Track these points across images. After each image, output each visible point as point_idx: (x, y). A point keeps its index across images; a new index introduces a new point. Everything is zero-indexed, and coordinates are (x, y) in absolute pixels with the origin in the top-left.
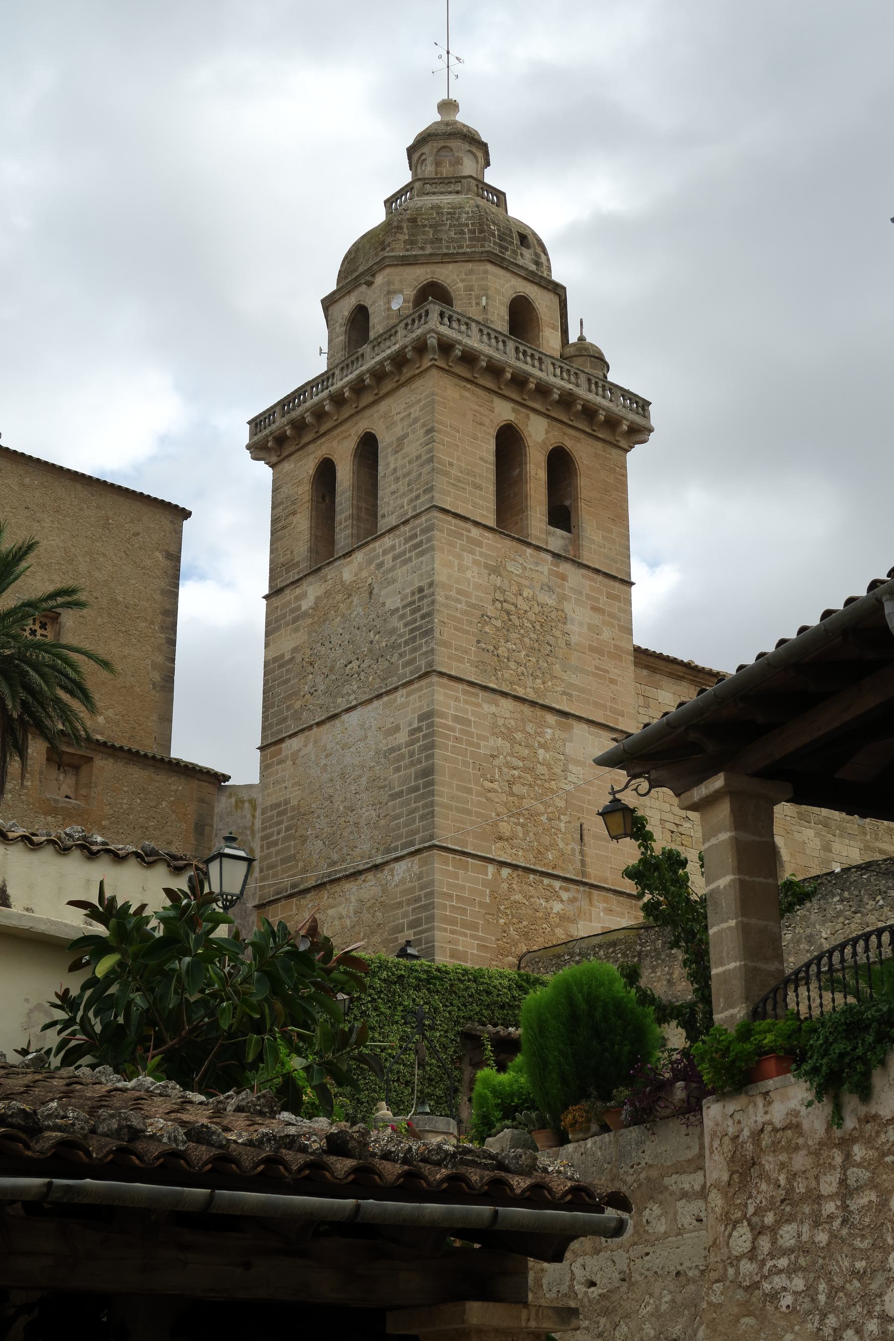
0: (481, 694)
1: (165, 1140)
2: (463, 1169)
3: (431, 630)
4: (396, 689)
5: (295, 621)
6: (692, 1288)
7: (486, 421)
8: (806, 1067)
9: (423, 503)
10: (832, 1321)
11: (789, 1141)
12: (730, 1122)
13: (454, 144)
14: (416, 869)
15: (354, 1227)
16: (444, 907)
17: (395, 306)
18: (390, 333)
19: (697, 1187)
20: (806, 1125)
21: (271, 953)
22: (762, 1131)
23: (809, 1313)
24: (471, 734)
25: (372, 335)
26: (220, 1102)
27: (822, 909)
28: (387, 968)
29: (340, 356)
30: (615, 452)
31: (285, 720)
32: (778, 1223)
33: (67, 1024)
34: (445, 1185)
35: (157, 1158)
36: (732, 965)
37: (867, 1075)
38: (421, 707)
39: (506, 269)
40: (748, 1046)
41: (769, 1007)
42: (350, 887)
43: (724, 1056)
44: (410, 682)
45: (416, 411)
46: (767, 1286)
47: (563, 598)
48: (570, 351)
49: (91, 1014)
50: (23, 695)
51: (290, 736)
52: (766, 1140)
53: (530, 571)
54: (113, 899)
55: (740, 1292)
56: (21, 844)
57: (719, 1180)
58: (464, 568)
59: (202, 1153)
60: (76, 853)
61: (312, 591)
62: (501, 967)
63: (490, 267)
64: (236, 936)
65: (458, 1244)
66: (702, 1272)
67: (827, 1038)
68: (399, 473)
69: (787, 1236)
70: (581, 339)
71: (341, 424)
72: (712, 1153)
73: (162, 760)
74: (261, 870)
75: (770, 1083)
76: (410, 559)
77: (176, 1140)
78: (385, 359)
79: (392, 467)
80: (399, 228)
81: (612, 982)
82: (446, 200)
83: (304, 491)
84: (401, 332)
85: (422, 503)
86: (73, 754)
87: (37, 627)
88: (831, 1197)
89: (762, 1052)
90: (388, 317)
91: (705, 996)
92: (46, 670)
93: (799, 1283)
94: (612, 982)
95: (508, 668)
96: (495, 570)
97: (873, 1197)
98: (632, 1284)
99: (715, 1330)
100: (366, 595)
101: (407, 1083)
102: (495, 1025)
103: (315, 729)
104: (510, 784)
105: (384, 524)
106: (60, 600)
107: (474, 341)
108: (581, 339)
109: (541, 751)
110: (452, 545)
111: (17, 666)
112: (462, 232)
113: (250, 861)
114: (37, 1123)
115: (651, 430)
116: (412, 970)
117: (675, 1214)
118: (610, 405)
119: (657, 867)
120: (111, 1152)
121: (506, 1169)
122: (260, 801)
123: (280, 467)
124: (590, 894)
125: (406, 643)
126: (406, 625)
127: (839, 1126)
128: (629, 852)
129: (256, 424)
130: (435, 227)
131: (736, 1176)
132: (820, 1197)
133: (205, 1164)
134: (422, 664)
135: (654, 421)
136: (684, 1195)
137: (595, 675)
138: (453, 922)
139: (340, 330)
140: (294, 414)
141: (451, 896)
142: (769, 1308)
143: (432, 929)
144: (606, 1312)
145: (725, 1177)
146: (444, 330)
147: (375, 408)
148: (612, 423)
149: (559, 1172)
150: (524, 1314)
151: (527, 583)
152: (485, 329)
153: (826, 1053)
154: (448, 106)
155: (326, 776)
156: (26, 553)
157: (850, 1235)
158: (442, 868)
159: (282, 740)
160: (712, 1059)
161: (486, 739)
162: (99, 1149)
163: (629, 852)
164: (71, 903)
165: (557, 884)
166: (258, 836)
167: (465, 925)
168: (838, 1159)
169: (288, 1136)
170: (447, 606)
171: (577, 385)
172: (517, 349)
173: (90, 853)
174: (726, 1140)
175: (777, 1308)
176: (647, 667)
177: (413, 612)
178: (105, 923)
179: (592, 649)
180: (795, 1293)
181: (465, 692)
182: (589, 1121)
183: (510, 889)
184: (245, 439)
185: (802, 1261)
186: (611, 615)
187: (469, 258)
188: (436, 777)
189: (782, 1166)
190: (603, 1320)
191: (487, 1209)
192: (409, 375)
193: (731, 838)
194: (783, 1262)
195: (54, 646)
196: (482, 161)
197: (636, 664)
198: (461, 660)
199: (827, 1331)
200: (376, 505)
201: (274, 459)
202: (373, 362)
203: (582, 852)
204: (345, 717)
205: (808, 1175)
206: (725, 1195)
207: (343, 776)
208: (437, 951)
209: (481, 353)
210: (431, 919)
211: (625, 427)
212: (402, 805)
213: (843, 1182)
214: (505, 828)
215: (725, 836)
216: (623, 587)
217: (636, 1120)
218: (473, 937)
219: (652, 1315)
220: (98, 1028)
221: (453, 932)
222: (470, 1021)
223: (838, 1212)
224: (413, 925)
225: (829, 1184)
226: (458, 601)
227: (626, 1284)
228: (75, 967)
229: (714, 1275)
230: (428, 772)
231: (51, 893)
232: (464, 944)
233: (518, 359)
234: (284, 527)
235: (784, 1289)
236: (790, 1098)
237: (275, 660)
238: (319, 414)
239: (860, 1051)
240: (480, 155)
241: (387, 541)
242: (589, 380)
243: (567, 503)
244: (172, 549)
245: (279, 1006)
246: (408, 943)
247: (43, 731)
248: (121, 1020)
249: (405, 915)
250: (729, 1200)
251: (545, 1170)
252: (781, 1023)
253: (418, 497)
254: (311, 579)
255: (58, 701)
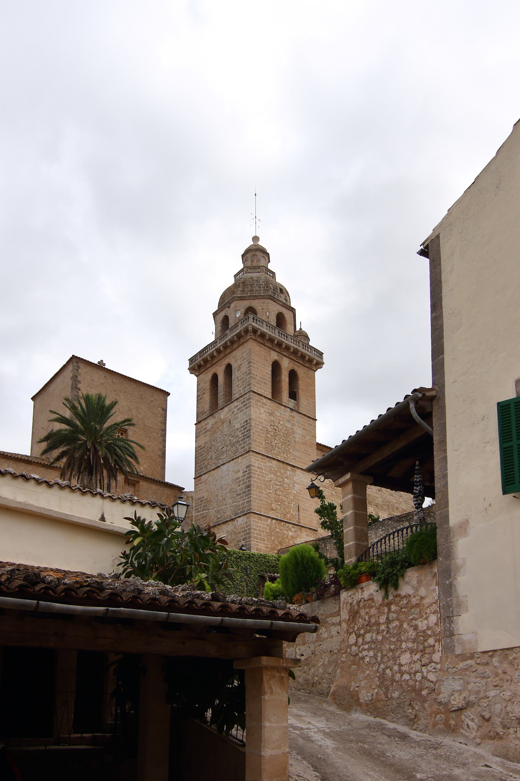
0: (266, 459)
1: (151, 594)
2: (260, 607)
3: (250, 436)
4: (238, 457)
5: (205, 433)
6: (335, 656)
7: (268, 359)
8: (376, 578)
9: (247, 389)
10: (382, 666)
11: (369, 604)
12: (350, 598)
13: (259, 254)
14: (245, 520)
15: (221, 628)
16: (254, 533)
17: (238, 316)
18: (236, 326)
19: (338, 621)
20: (375, 599)
21: (194, 537)
22: (360, 601)
23: (375, 663)
24: (263, 473)
25: (230, 327)
26: (176, 588)
27: (376, 534)
28: (236, 554)
29: (219, 335)
30: (311, 372)
31: (202, 468)
32: (365, 633)
33: (126, 563)
34: (254, 612)
35: (148, 600)
36: (351, 543)
37: (397, 580)
38: (247, 463)
39: (275, 302)
40: (356, 571)
41: (363, 558)
42: (224, 526)
43: (348, 575)
44: (243, 454)
45: (245, 355)
46: (360, 655)
47: (293, 425)
48: (297, 334)
49: (133, 560)
50: (115, 457)
51: (204, 474)
52: (362, 604)
53: (282, 414)
54: (139, 517)
55: (352, 657)
56: (108, 499)
57: (345, 618)
58: (262, 413)
59: (165, 599)
60: (128, 503)
61: (211, 422)
62: (274, 554)
63: (270, 301)
64: (183, 531)
65: (257, 636)
66: (339, 651)
67: (384, 567)
68: (239, 378)
69: (368, 638)
70: (301, 329)
71: (220, 360)
72: (343, 609)
73: (162, 482)
74: (195, 521)
75: (364, 584)
76: (243, 410)
77: (155, 594)
78: (234, 336)
79: (237, 376)
80: (239, 285)
81: (310, 551)
82: (255, 275)
83: (207, 385)
84: (240, 325)
85: (247, 390)
86: (133, 480)
87: (120, 435)
88: (383, 624)
89: (361, 573)
90: (235, 320)
91: (342, 555)
92: (122, 448)
93: (371, 653)
94: (310, 551)
95: (275, 450)
96: (271, 414)
97: (398, 624)
98: (315, 655)
99: (343, 670)
100: (228, 423)
101: (242, 592)
102: (270, 573)
103: (212, 472)
104: (276, 491)
105: (234, 397)
106: (126, 423)
107: (264, 329)
108: (301, 329)
109: (286, 479)
110: (257, 405)
111: (113, 447)
112: (260, 287)
113: (187, 506)
114: (102, 586)
115: (323, 364)
116: (244, 554)
117: (330, 631)
118: (310, 354)
119: (326, 508)
120: (130, 597)
121: (276, 608)
122: (194, 497)
123: (199, 376)
124: (301, 529)
125: (242, 440)
126: (242, 434)
127: (387, 599)
128: (316, 503)
129: (191, 360)
130: (251, 285)
131: (351, 617)
132: (380, 624)
133: (166, 603)
134: (247, 448)
135: (325, 360)
136: (334, 624)
137: (303, 452)
138: (257, 538)
139: (219, 325)
140: (204, 357)
141: (256, 529)
142: (361, 662)
143: (250, 541)
144: (307, 665)
145: (348, 618)
146: (254, 324)
147: (231, 354)
148: (310, 361)
149: (294, 609)
150: (282, 661)
151: (282, 419)
152: (268, 324)
153: (383, 573)
154: (256, 239)
155: (216, 488)
156: (114, 405)
157: (389, 636)
158: (254, 519)
159: (201, 476)
160: (344, 576)
161: (268, 475)
162: (125, 597)
163: (316, 503)
164: (125, 518)
165: (291, 526)
166: (194, 509)
167: (261, 539)
168: (386, 610)
169: (197, 594)
170: (255, 427)
171: (299, 346)
172: (279, 332)
173: (133, 503)
174: (348, 605)
175: (364, 662)
176: (320, 450)
177: (244, 429)
178: (137, 526)
179: (303, 443)
180: (370, 657)
181: (261, 458)
182: (302, 599)
183: (275, 527)
184: (187, 365)
185: (373, 646)
186: (309, 431)
187: (263, 297)
188: (252, 488)
189: (367, 613)
190: (306, 667)
191: (269, 621)
192: (242, 341)
193: (352, 497)
194: (366, 647)
195: (124, 440)
196: (267, 260)
197: (317, 449)
198: (259, 446)
199: (380, 670)
200: (231, 391)
201: (197, 374)
202: (230, 337)
203: (299, 515)
204: (222, 467)
205: (376, 616)
206: (347, 624)
207: (221, 488)
208: (252, 548)
209: (267, 333)
210: (250, 537)
211: (315, 362)
212: (240, 498)
213: (387, 618)
214: (274, 506)
215: (350, 496)
216: (313, 421)
217: (318, 599)
218: (264, 544)
219: (322, 665)
220: (136, 565)
221: (257, 542)
222: (262, 569)
223: (386, 629)
224: (244, 539)
225: (383, 619)
226: (259, 425)
227: (313, 655)
228: (128, 542)
229: (343, 651)
230: (249, 486)
231: (119, 517)
232: (261, 546)
233: (279, 336)
234: (201, 399)
235: (367, 656)
236: (371, 589)
237: (199, 447)
238: (212, 356)
239: (395, 572)
240: (267, 258)
241: (235, 403)
242: (303, 344)
243: (295, 390)
244: (164, 407)
245: (197, 555)
246: (243, 546)
247: (124, 473)
248: (144, 563)
249: (242, 536)
250: (348, 625)
251: (289, 608)
252: (367, 563)
253: (245, 387)
254: (210, 417)
255: (127, 460)
